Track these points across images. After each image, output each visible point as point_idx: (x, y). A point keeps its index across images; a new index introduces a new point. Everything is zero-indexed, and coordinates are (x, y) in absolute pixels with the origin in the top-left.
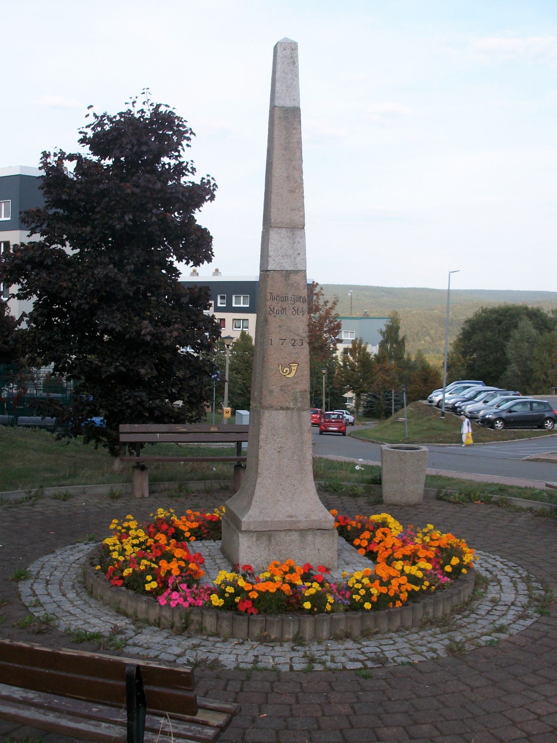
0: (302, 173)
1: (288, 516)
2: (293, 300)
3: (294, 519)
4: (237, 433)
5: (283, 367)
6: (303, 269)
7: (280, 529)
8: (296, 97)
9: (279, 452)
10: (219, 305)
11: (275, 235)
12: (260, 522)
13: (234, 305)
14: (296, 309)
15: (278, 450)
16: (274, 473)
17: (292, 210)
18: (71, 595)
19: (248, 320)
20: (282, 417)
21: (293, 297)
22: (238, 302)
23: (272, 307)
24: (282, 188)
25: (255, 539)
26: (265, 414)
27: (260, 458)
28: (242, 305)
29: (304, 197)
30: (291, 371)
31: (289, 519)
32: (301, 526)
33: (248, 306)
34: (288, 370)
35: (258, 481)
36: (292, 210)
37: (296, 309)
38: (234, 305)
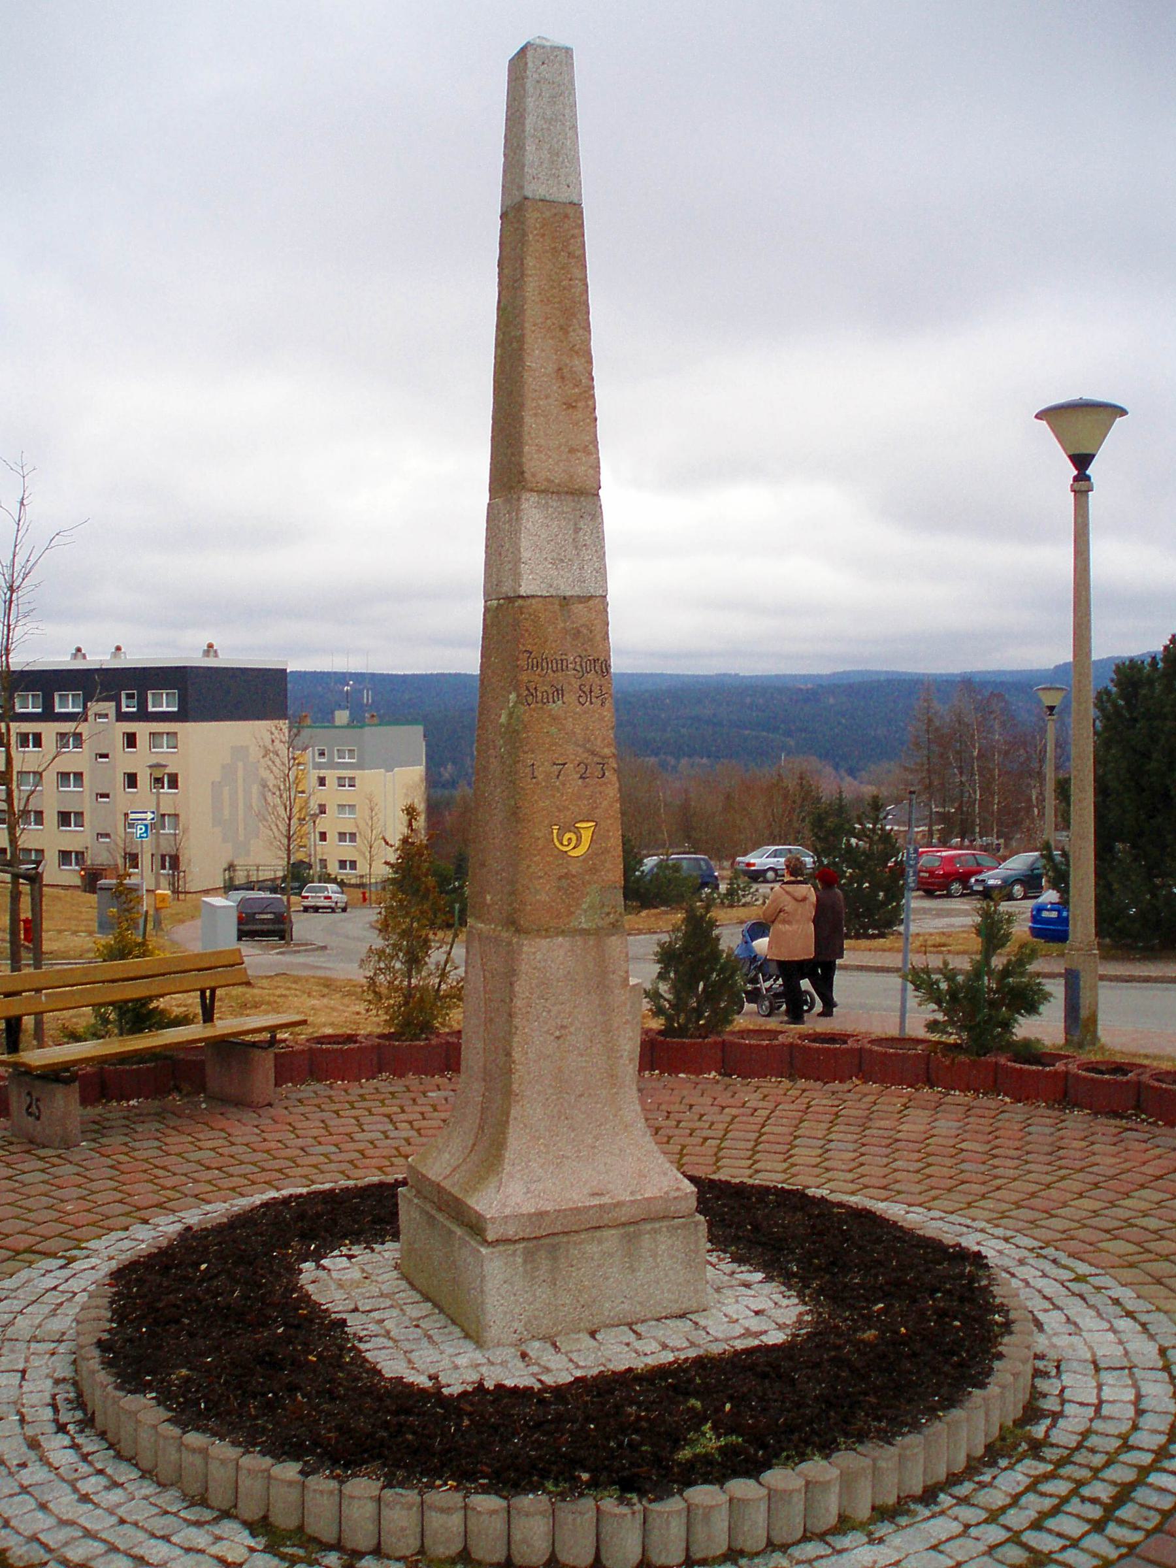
0: (590, 362)
1: (594, 1194)
2: (578, 668)
3: (606, 1200)
4: (113, 981)
5: (563, 830)
6: (601, 592)
7: (575, 1228)
8: (575, 183)
9: (558, 1038)
10: (124, 709)
11: (534, 511)
12: (530, 1215)
13: (151, 709)
14: (587, 689)
15: (557, 1034)
16: (550, 1091)
17: (572, 451)
18: (58, 1449)
19: (176, 733)
20: (562, 953)
21: (578, 660)
22: (64, 704)
23: (532, 685)
24: (547, 397)
25: (520, 1260)
26: (525, 949)
27: (516, 1055)
28: (30, 710)
29: (596, 419)
30: (579, 839)
31: (596, 1201)
32: (624, 1214)
33: (176, 709)
34: (574, 837)
35: (513, 1113)
36: (572, 451)
37: (587, 689)
38: (151, 709)
